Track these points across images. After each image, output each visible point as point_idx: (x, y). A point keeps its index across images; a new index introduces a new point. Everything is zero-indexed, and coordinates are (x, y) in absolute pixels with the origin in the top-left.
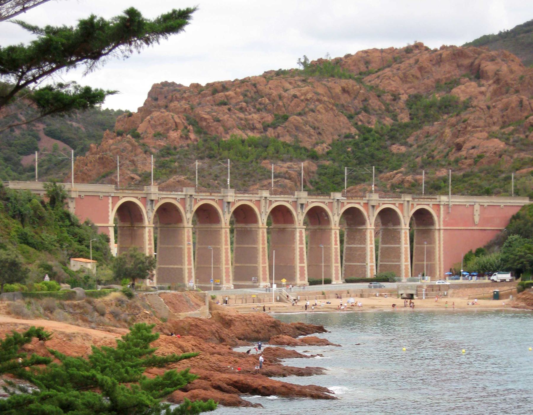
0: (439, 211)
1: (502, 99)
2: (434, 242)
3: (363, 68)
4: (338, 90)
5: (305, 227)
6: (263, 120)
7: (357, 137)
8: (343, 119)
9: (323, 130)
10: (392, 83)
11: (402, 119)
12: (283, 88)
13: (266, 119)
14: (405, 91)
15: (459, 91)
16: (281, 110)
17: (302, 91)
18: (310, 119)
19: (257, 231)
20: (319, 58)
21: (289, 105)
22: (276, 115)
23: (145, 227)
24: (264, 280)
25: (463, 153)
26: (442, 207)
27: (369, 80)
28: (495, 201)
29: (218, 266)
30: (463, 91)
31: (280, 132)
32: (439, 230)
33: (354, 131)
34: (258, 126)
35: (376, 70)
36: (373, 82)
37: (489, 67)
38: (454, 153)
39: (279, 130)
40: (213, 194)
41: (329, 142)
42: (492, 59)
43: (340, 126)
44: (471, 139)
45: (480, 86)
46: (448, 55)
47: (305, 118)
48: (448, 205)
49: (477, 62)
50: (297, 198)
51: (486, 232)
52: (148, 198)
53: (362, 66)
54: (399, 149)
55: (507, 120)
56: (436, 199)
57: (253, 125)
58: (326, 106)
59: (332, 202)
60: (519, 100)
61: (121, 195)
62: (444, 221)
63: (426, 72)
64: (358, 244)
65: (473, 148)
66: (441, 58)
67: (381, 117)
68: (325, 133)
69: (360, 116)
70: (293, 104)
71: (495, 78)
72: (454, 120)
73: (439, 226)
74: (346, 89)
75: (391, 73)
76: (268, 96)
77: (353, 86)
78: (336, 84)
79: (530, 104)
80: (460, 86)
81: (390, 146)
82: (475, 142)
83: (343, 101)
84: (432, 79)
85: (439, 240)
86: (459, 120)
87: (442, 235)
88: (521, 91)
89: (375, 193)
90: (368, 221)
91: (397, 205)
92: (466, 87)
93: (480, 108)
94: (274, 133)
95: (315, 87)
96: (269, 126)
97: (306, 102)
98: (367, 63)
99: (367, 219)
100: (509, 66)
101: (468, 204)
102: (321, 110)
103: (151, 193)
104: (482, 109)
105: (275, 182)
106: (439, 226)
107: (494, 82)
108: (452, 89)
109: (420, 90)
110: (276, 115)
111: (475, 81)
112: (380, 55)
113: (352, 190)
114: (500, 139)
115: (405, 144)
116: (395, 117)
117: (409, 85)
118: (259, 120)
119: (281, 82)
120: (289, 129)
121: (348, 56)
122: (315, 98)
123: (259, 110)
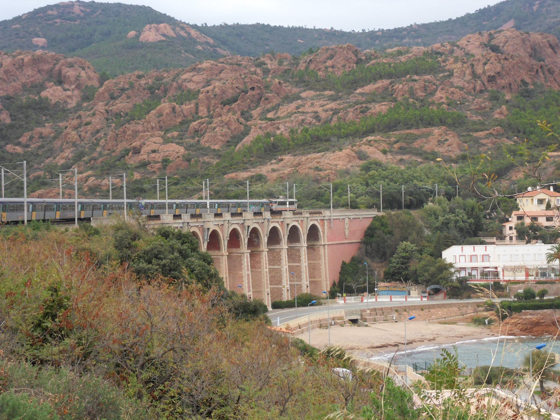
0: (323, 226)
2: (320, 259)
5: (250, 251)
11: (4, 120)
15: (49, 96)
19: (219, 259)
26: (325, 221)
30: (52, 95)
37: (70, 73)
38: (132, 156)
42: (71, 66)
45: (65, 90)
46: (30, 60)
49: (57, 67)
55: (163, 125)
63: (12, 75)
65: (154, 151)
66: (23, 63)
71: (76, 83)
72: (75, 122)
73: (324, 241)
80: (47, 90)
84: (19, 82)
85: (325, 256)
88: (132, 97)
92: (53, 90)
93: (100, 112)
100: (86, 73)
101: (341, 218)
104: (102, 113)
106: (324, 241)
107: (76, 87)
108: (40, 92)
115: (19, 144)
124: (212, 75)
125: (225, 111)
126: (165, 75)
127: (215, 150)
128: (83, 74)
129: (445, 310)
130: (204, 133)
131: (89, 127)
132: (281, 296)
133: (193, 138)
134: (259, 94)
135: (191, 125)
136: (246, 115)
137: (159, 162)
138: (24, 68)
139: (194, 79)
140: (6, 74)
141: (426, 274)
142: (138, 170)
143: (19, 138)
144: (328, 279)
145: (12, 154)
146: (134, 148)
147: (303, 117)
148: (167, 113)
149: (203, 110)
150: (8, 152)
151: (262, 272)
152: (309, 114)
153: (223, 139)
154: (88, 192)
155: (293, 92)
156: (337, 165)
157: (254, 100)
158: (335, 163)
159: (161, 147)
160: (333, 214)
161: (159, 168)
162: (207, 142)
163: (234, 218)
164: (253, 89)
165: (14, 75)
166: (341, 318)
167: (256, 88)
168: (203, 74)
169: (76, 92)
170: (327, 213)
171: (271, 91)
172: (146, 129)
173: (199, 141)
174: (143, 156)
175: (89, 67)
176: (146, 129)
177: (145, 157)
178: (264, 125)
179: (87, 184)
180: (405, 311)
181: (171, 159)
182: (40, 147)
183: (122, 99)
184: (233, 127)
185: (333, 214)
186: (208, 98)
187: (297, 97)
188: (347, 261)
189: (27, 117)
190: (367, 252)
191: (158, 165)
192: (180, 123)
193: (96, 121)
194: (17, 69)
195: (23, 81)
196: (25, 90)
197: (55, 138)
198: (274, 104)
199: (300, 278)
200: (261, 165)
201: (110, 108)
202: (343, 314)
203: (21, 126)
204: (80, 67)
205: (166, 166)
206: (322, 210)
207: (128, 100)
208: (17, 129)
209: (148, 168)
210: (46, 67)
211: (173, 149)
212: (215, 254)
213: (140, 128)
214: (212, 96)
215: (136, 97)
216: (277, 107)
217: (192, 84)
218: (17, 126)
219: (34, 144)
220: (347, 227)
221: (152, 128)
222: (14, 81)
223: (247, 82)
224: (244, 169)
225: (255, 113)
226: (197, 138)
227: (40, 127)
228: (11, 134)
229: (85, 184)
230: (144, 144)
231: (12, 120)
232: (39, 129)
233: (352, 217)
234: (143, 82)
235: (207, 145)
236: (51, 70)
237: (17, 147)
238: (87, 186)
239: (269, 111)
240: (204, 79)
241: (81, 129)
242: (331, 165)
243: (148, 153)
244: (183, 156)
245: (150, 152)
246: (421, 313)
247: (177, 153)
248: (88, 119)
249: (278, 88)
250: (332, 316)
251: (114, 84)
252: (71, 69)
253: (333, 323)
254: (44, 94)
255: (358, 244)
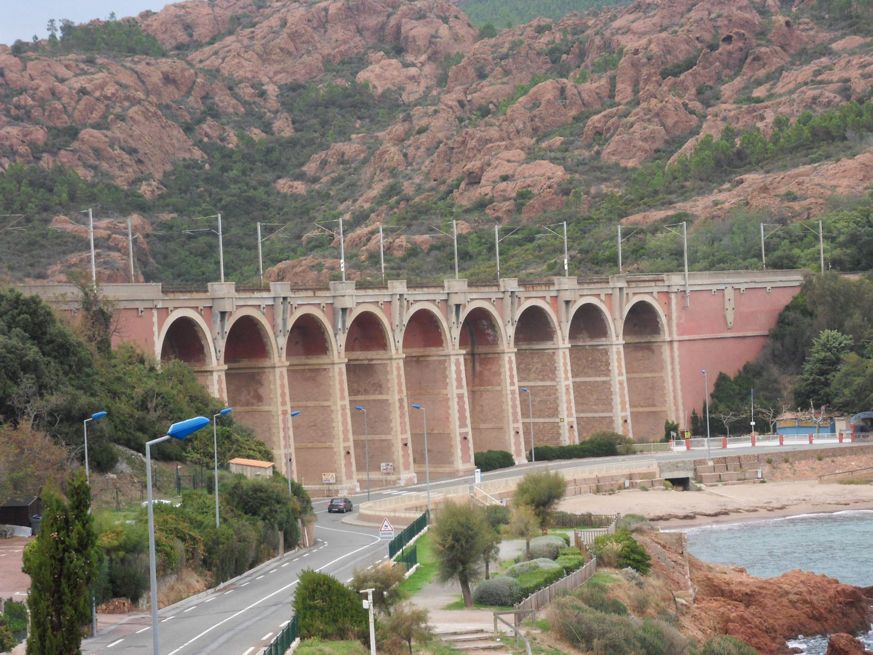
0: (668, 304)
1: (482, 87)
2: (662, 368)
3: (183, 37)
4: (156, 78)
5: (464, 352)
6: (28, 138)
7: (207, 166)
8: (177, 133)
9: (146, 154)
10: (245, 63)
12: (56, 77)
13: (33, 136)
14: (270, 78)
16: (58, 118)
17: (95, 82)
18: (118, 134)
20: (94, 18)
21: (74, 108)
22: (49, 129)
23: (211, 372)
24: (407, 468)
25: (484, 189)
26: (673, 296)
27: (198, 59)
28: (757, 279)
29: (328, 444)
30: (379, 77)
31: (65, 160)
32: (671, 342)
33: (198, 154)
34: (22, 149)
35: (207, 39)
36: (208, 62)
37: (418, 31)
38: (465, 190)
39: (64, 156)
40: (318, 293)
41: (158, 176)
43: (173, 145)
44: (494, 162)
45: (406, 65)
46: (339, 9)
47: (109, 133)
48: (685, 291)
49: (393, 21)
50: (448, 294)
51: (747, 341)
52: (216, 311)
53: (180, 34)
54: (291, 187)
55: (539, 124)
56: (663, 281)
57: (11, 146)
58: (143, 109)
59: (502, 299)
60: (559, 86)
61: (170, 305)
62: (678, 325)
63: (303, 42)
64: (535, 379)
65: (505, 178)
66: (326, 16)
67: (240, 126)
68: (150, 160)
69: (204, 126)
70: (82, 105)
71: (429, 51)
72: (398, 128)
73: (671, 334)
74: (171, 76)
75: (239, 45)
76: (31, 92)
77: (183, 70)
78: (152, 68)
79: (579, 93)
80: (370, 67)
81: (274, 182)
82: (506, 169)
83: (166, 100)
85: (672, 363)
86: (410, 130)
87: (676, 353)
88: (514, 72)
89: (570, 275)
90: (559, 332)
91: (603, 297)
92: (382, 68)
93: (446, 105)
94: (54, 161)
95: (114, 72)
96: (862, 127)
97: (106, 102)
98: (188, 28)
99: (558, 328)
101: (714, 288)
102: (137, 117)
103: (212, 372)
104: (451, 107)
105: (98, 256)
106: (671, 334)
107: (429, 58)
108: (357, 73)
109: (298, 76)
110: (49, 129)
111: (396, 58)
112: (211, 12)
113: (293, 267)
114: (553, 160)
115: (301, 177)
116: (267, 128)
117: (277, 67)
118: (21, 138)
119: (49, 65)
120: (82, 154)
121: (147, 14)
122: (121, 93)
123: (17, 118)
124: (672, 16)
125: (666, 88)
126: (591, 22)
127: (625, 169)
128: (444, 30)
129: (864, 458)
130: (612, 136)
131: (423, 138)
132: (559, 438)
133: (589, 146)
134: (741, 49)
135: (589, 122)
136: (708, 93)
137: (510, 199)
138: (328, 26)
139: (634, 26)
140: (293, 40)
141: (846, 391)
142: (467, 216)
143: (303, 164)
144: (681, 408)
145: (285, 196)
146: (470, 173)
147: (816, 92)
148: (548, 101)
149: (624, 90)
150: (279, 193)
151: (504, 393)
152: (831, 86)
153: (646, 146)
154: (366, 263)
155: (818, 41)
156: (835, 187)
157: (732, 61)
158: (834, 182)
159: (519, 169)
160: (691, 282)
161: (509, 211)
162: (614, 153)
163: (412, 291)
164: (728, 39)
165: (308, 42)
166: (649, 476)
167: (735, 37)
168: (654, 16)
169: (428, 69)
170: (675, 280)
171: (768, 41)
172: (505, 135)
173: (598, 153)
174: (484, 189)
175: (456, 17)
176: (505, 135)
177: (488, 190)
178: (732, 113)
179: (367, 247)
180: (786, 461)
181: (536, 191)
182: (334, 181)
183: (495, 77)
184: (670, 122)
185: (691, 282)
186: (635, 65)
187: (825, 51)
188: (731, 374)
189: (324, 123)
190: (774, 356)
191: (507, 205)
192: (574, 118)
193: (438, 124)
194: (314, 28)
195: (326, 52)
196: (328, 70)
197: (365, 161)
198: (773, 68)
199: (610, 404)
200: (699, 194)
201: (469, 97)
202: (654, 468)
203: (311, 142)
204: (439, 17)
205: (523, 205)
206: (664, 276)
207: (505, 79)
208: (303, 147)
209: (487, 211)
210: (372, 22)
211: (542, 172)
212: (379, 357)
213: (494, 132)
214: (644, 60)
215: (521, 72)
216: (777, 74)
217: (631, 36)
218: (303, 142)
219: (326, 175)
220: (729, 306)
221: (518, 132)
222: (309, 52)
223: (720, 27)
224: (663, 204)
225: (726, 90)
226: (596, 148)
227: (341, 141)
228: (288, 159)
229: (364, 248)
230: (489, 165)
231: (297, 130)
232: (340, 146)
233: (743, 287)
234: (545, 38)
235: (614, 159)
236: (382, 27)
237: (296, 183)
238: (367, 250)
239: (759, 83)
240: (654, 25)
241: (410, 142)
242: (823, 187)
243: (494, 182)
244: (559, 185)
245: (498, 179)
246: (817, 464)
247: (549, 178)
248: (423, 122)
249: (784, 35)
250: (627, 472)
251: (492, 47)
252: (421, 21)
253: (627, 484)
254: (363, 76)
255: (761, 340)
